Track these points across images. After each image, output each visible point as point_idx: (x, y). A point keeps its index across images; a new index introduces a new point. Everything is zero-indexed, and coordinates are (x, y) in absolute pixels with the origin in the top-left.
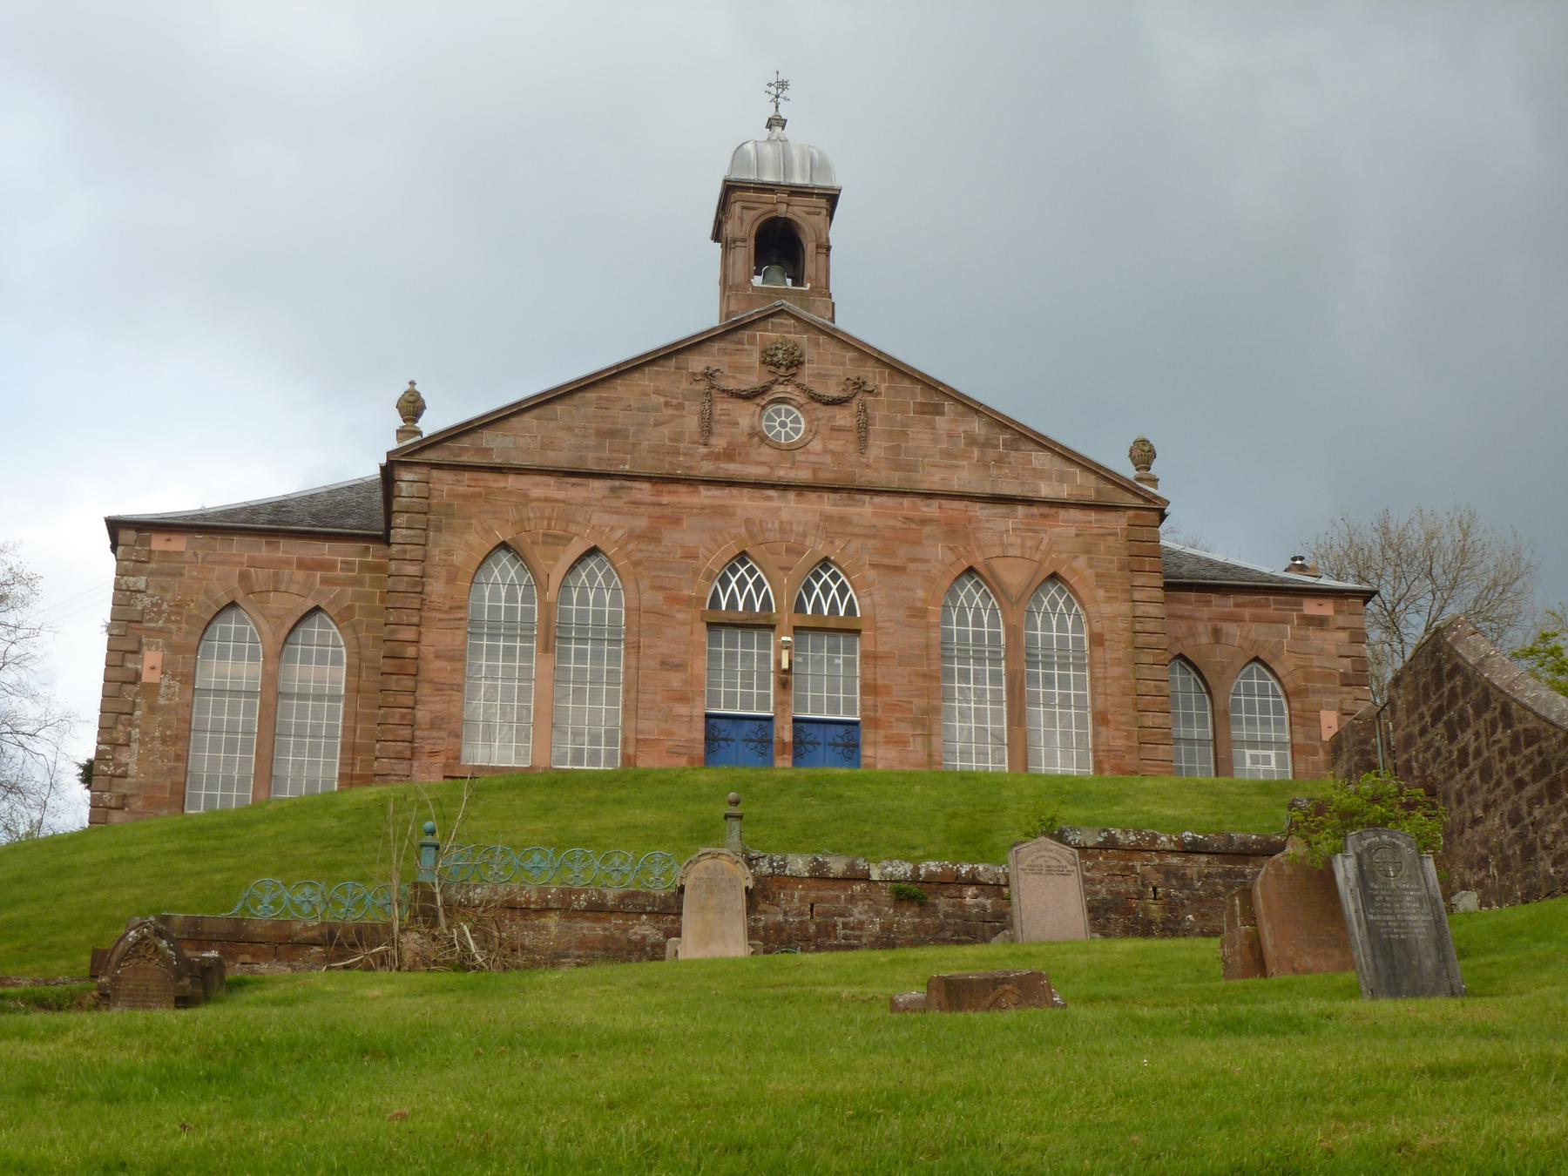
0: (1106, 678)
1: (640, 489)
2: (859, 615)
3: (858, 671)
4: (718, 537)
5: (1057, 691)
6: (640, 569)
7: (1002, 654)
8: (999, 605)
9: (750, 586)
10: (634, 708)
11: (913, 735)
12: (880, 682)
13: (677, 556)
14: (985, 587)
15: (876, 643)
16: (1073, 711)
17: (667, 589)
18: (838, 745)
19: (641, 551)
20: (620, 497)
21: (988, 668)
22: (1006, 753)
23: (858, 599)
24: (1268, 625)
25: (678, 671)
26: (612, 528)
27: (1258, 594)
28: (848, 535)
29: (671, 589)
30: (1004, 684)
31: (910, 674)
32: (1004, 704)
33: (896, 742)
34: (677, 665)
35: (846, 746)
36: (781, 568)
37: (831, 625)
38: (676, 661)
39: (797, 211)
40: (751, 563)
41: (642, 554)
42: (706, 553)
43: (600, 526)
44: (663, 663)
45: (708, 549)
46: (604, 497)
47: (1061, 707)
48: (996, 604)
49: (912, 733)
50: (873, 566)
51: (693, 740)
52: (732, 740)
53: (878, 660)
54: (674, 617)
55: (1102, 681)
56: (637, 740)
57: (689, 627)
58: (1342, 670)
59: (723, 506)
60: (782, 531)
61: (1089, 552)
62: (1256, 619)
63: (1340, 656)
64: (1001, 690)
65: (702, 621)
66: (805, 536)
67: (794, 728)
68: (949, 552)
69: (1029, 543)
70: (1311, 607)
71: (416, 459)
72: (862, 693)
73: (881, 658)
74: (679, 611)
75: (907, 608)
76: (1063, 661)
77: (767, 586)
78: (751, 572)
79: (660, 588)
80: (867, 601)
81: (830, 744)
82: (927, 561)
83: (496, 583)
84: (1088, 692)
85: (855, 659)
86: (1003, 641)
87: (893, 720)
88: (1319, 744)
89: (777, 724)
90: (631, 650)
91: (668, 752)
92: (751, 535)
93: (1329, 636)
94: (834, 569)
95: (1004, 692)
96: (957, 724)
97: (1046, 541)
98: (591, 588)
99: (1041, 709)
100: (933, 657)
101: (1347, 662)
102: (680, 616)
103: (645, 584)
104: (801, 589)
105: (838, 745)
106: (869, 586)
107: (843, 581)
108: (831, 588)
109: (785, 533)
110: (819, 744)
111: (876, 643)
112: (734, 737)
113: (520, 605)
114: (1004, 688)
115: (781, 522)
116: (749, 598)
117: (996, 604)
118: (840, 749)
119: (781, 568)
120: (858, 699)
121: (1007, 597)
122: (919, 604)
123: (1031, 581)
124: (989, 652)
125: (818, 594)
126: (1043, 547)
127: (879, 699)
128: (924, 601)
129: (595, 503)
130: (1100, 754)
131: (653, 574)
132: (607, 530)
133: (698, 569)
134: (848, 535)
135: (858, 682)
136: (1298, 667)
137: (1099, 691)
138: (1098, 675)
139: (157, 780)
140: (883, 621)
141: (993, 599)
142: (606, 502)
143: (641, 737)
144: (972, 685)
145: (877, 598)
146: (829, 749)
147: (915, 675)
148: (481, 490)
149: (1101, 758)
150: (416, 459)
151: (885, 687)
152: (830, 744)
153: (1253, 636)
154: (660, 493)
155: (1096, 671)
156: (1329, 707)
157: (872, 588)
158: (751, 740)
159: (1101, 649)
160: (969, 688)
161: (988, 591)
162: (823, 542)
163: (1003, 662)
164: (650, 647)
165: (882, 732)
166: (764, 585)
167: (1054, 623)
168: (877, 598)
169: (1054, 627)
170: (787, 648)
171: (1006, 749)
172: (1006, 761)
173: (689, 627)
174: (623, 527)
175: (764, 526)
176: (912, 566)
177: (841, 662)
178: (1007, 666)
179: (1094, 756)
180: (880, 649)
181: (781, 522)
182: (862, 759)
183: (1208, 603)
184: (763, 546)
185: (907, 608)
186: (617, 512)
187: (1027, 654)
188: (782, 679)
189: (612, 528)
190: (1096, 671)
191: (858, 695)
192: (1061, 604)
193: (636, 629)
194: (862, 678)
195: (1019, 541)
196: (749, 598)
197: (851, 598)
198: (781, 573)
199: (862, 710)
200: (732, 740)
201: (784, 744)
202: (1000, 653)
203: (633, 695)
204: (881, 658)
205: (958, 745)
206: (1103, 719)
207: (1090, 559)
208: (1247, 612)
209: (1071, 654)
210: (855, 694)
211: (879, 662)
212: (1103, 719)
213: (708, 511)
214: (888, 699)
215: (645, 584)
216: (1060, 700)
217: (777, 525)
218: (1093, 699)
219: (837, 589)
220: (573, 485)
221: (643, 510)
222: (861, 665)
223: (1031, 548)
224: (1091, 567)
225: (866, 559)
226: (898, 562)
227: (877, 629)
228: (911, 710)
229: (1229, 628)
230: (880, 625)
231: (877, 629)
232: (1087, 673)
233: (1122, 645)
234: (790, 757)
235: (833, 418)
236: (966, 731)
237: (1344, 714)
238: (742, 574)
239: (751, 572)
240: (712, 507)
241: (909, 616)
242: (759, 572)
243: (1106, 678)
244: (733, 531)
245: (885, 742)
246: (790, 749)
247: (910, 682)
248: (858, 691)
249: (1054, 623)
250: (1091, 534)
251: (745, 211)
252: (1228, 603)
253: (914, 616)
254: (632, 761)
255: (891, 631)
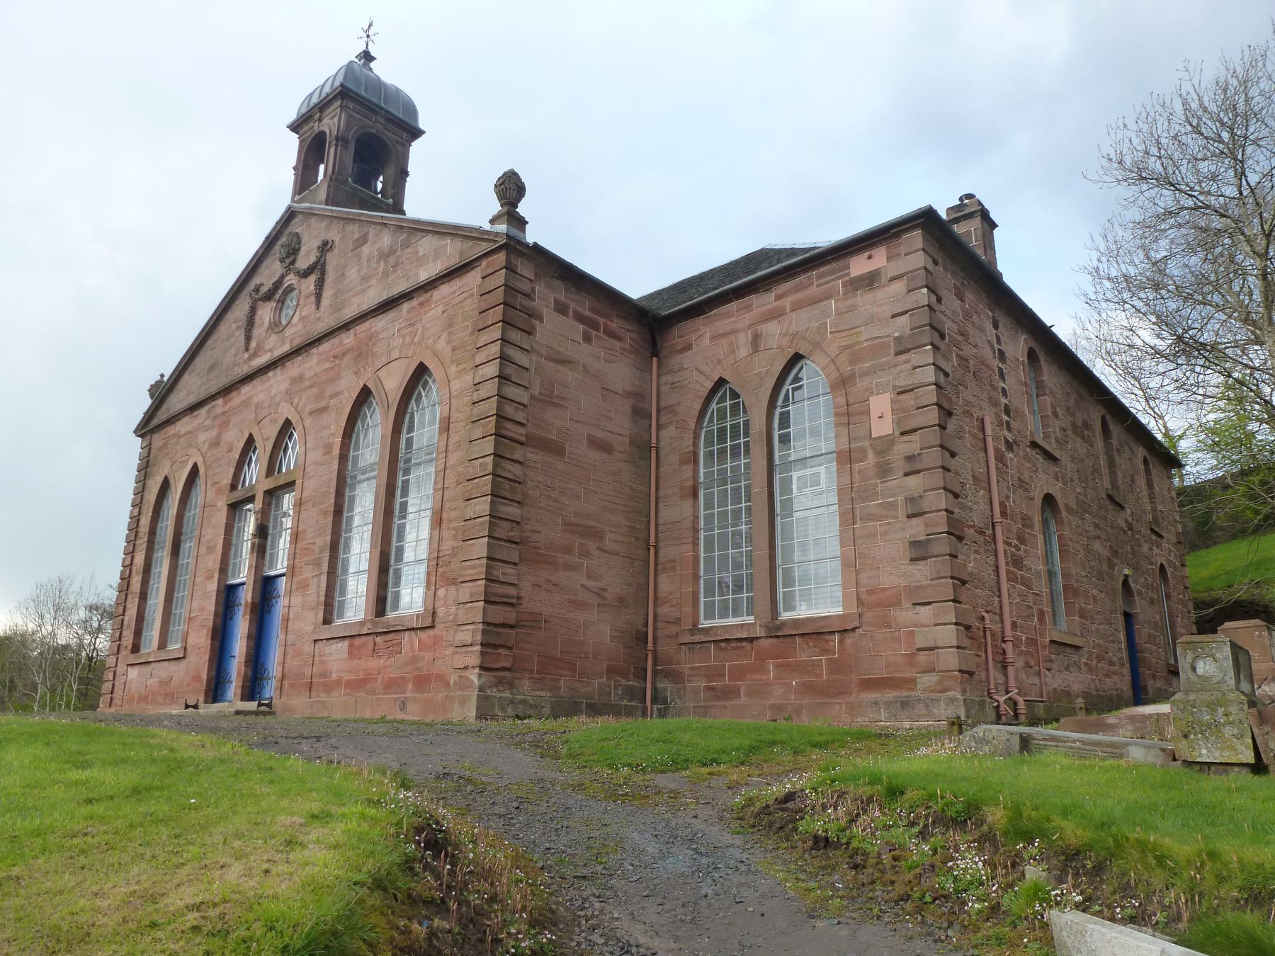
24: (809, 308)
27: (796, 275)
39: (389, 135)
58: (896, 334)
62: (797, 307)
63: (894, 316)
70: (859, 266)
71: (155, 422)
88: (867, 444)
93: (880, 294)
101: (903, 320)
136: (844, 348)
148: (655, 709)
150: (155, 422)
153: (793, 329)
156: (881, 389)
183: (748, 308)
208: (787, 302)
229: (772, 328)
233: (463, 424)
235: (341, 343)
237: (899, 393)
251: (129, 668)
252: (762, 302)
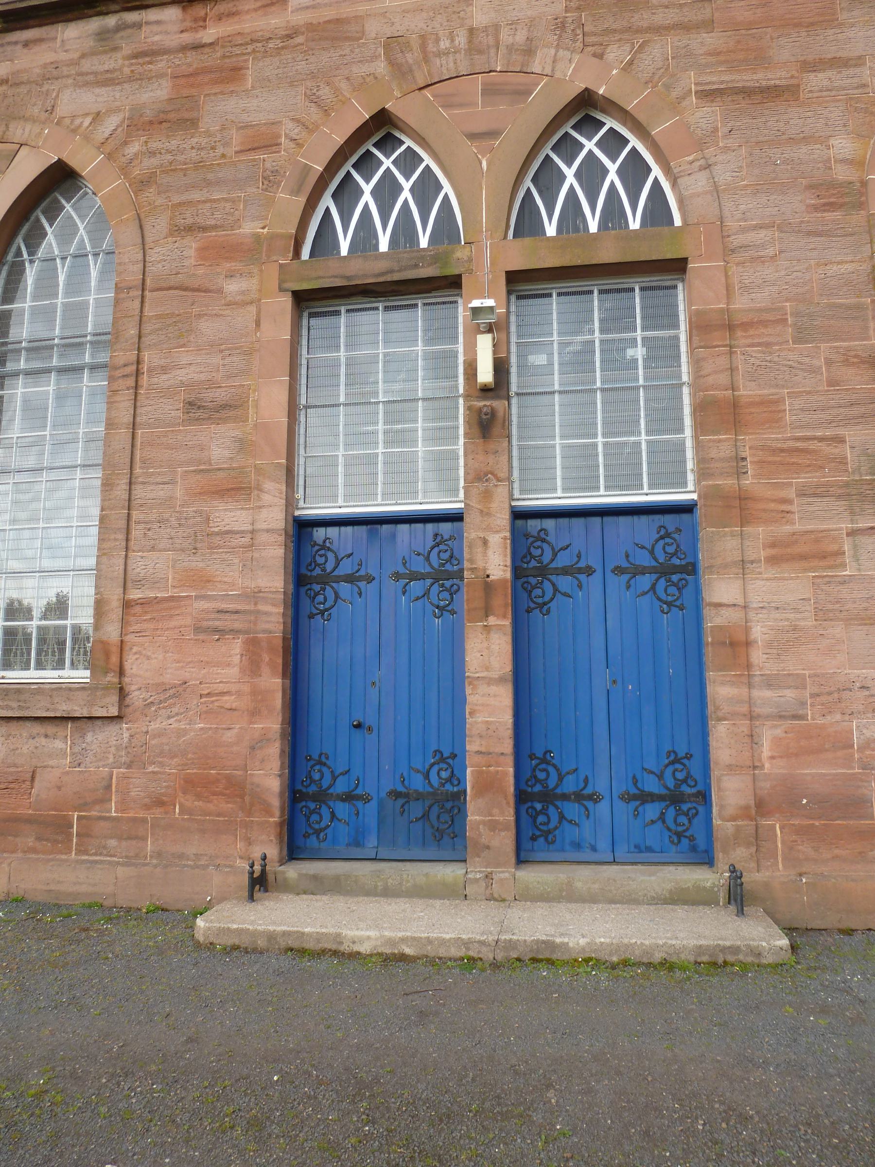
1: (158, 22)
2: (678, 222)
3: (684, 368)
4: (325, 92)
6: (150, 193)
9: (612, 176)
10: (122, 523)
11: (851, 533)
12: (747, 391)
13: (230, 151)
15: (729, 288)
17: (204, 229)
18: (642, 571)
19: (152, 154)
20: (115, 49)
23: (674, 185)
25: (225, 420)
26: (97, 117)
28: (640, 31)
29: (215, 227)
31: (829, 362)
33: (803, 557)
34: (225, 406)
35: (664, 571)
36: (473, 136)
37: (608, 254)
38: (221, 395)
40: (408, 143)
41: (155, 161)
42: (295, 131)
43: (74, 117)
44: (191, 404)
45: (297, 121)
46: (83, 56)
50: (708, 95)
51: (255, 595)
52: (370, 579)
53: (739, 333)
54: (220, 291)
56: (127, 605)
57: (253, 309)
59: (338, 21)
60: (473, 49)
65: (281, 290)
66: (529, 51)
67: (513, 530)
72: (700, 428)
73: (746, 326)
74: (230, 276)
77: (447, 188)
78: (409, 161)
79: (190, 229)
80: (697, 183)
81: (619, 570)
85: (677, 338)
87: (791, 493)
89: (471, 531)
90: (122, 384)
91: (198, 630)
92: (400, 70)
94: (610, 123)
102: (232, 287)
103: (157, 226)
104: (528, 183)
105: (642, 571)
106: (700, 145)
107: (634, 150)
108: (605, 171)
109: (480, 52)
110: (589, 571)
111: (729, 288)
112: (372, 572)
115: (471, 31)
116: (405, 222)
118: (645, 581)
119: (473, 136)
120: (689, 443)
122: (842, 173)
125: (406, 201)
127: (748, 440)
129: (65, 70)
131: (176, 199)
132: (87, 121)
133: (275, 172)
134: (640, 31)
135: (686, 400)
140: (743, 230)
142: (87, 65)
143: (135, 594)
145: (723, 175)
146: (616, 582)
147: (846, 362)
151: (763, 402)
152: (619, 570)
154: (201, 23)
157: (710, 151)
158: (415, 576)
162: (576, 57)
164: (164, 370)
165: (760, 532)
166: (649, 170)
168: (723, 175)
170: (490, 330)
173: (253, 309)
174: (118, 110)
175: (431, 47)
176: (816, 80)
177: (639, 353)
180: (741, 303)
181: (471, 31)
182: (707, 612)
184: (427, 93)
185: (810, 187)
186: (107, 80)
188: (480, 410)
189: (97, 117)
191: (688, 432)
193: (133, 332)
194: (696, 386)
196: (405, 222)
198: (474, 148)
199: (703, 473)
200: (370, 579)
201: (488, 587)
203: (121, 491)
204: (746, 326)
210: (681, 430)
211: (741, 338)
213: (300, 39)
214: (773, 437)
215: (157, 226)
217: (461, 40)
219: (412, 190)
220: (26, 44)
221: (161, 64)
222: (692, 349)
225: (690, 80)
226: (776, 77)
227: (728, 252)
228: (842, 461)
230: (737, 240)
231: (728, 252)
234: (507, 623)
238: (590, 152)
239: (409, 161)
240: (311, 27)
241: (816, 208)
242: (428, 160)
244: (360, 70)
245: (773, 560)
246: (503, 600)
247: (832, 383)
248: (688, 421)
253: (830, 206)
254: (114, 659)
255: (770, 252)
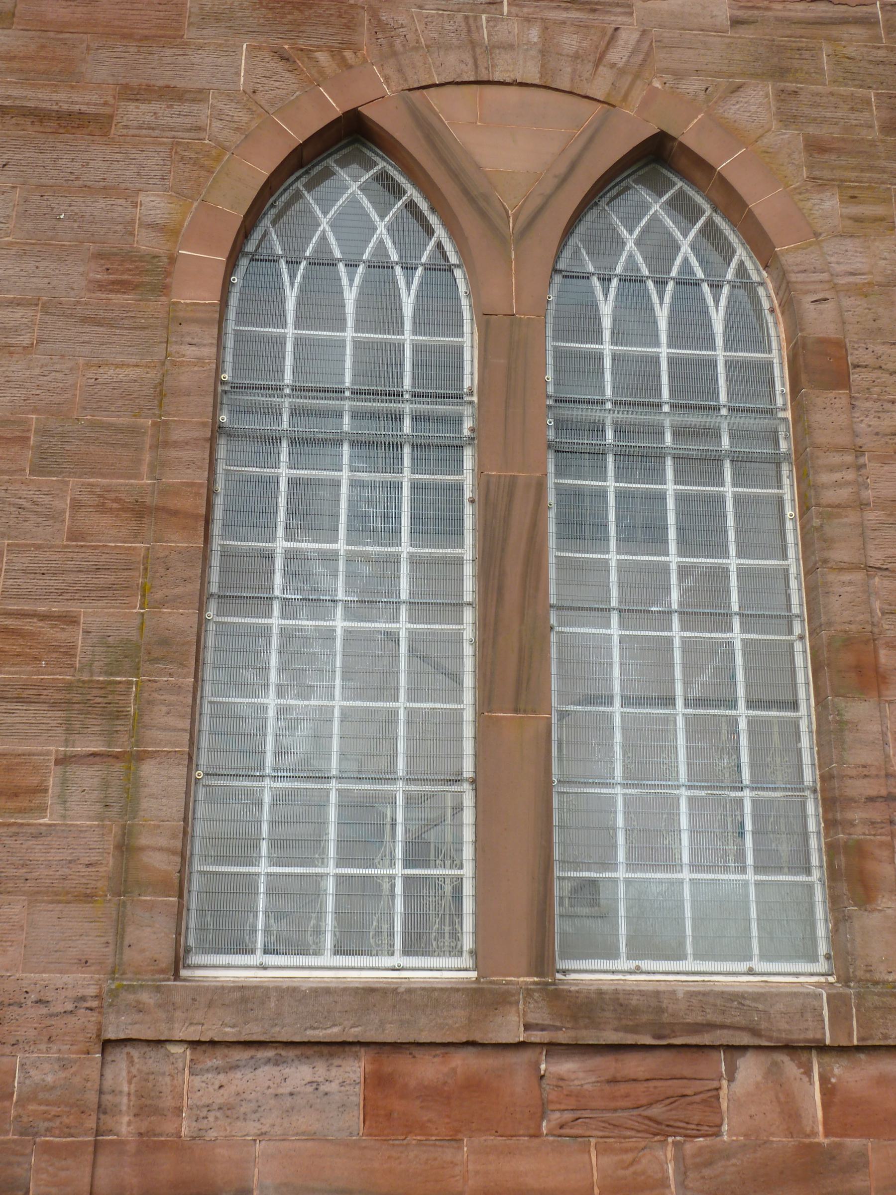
0: (863, 505)
5: (673, 559)
7: (467, 424)
8: (461, 251)
11: (63, 761)
14: (412, 192)
16: (737, 635)
21: (407, 477)
22: (468, 816)
30: (469, 538)
31: (76, 505)
32: (468, 615)
47: (689, 618)
48: (448, 247)
49: (56, 748)
55: (852, 517)
61: (781, 73)
64: (459, 562)
68: (278, 66)
69: (570, 42)
75: (99, 256)
76: (694, 447)
82: (199, 96)
83: (687, 283)
84: (793, 562)
86: (470, 378)
95: (468, 570)
96: (271, 701)
97: (628, 37)
98: (661, 284)
99: (615, 631)
100: (178, 434)
113: (290, 331)
114: (468, 550)
117: (448, 247)
121: (483, 215)
123: (573, 167)
124: (416, 418)
126: (617, 55)
128: (170, 231)
130: (857, 815)
137: (841, 554)
138: (830, 496)
139: (193, 915)
141: (440, 232)
144: (341, 546)
147: (102, 508)
149: (859, 833)
155: (825, 478)
159: (841, 398)
160: (330, 558)
161: (423, 206)
163: (468, 455)
166: (734, 251)
167: (662, 316)
169: (663, 325)
171: (468, 800)
172: (468, 852)
178: (480, 471)
179: (830, 824)
185: (99, 256)
187: (560, 425)
190: (825, 478)
192: (685, 248)
195: (534, 34)
197: (741, 264)
202: (458, 420)
205: (268, 789)
206: (859, 669)
207: (783, 95)
209: (724, 422)
212: (859, 669)
216: (684, 592)
218: (813, 592)
223: (576, 57)
224: (788, 119)
228: (69, 651)
232: (788, 491)
236: (305, 729)
241: (101, 286)
243: (863, 505)
249: (662, 316)
250: (780, 20)
253: (122, 286)
255: (25, 339)
